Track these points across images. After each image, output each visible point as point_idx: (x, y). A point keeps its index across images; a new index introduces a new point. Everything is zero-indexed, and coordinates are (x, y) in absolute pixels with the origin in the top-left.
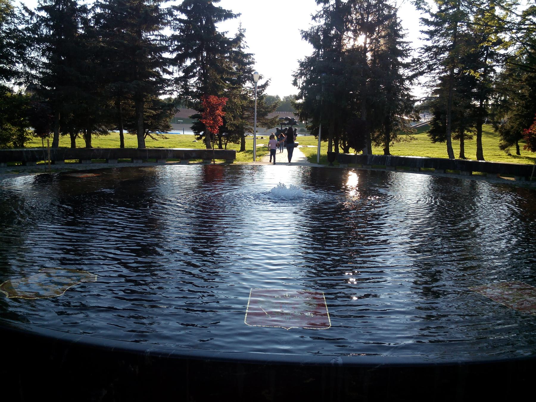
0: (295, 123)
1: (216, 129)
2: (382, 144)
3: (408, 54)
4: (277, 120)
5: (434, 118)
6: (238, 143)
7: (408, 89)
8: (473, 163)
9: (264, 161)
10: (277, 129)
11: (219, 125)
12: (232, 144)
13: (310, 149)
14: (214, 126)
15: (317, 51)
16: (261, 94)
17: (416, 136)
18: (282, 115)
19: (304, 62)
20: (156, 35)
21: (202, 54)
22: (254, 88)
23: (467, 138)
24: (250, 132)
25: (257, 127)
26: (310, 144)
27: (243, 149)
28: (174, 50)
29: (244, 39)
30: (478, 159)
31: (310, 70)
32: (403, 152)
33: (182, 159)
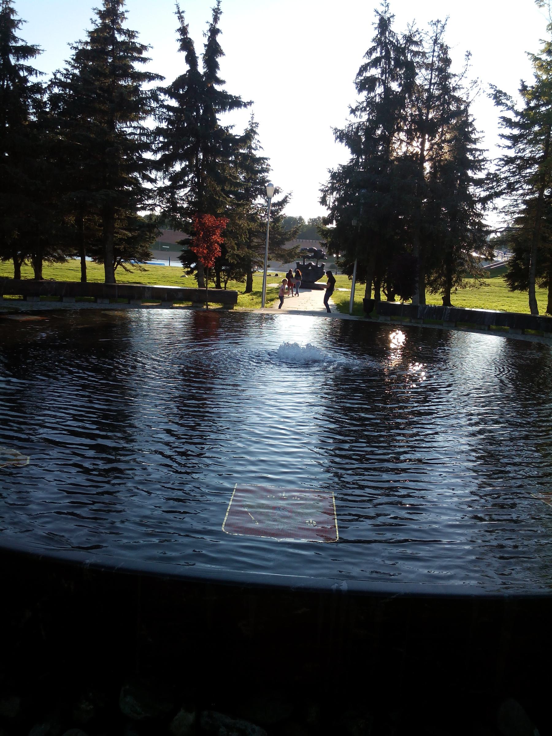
4: (298, 251)
6: (243, 282)
10: (298, 264)
11: (216, 255)
12: (234, 282)
13: (341, 294)
14: (209, 257)
16: (278, 214)
17: (488, 281)
19: (336, 173)
20: (134, 127)
24: (260, 266)
25: (269, 259)
26: (342, 287)
27: (249, 289)
32: (469, 302)
33: (163, 300)
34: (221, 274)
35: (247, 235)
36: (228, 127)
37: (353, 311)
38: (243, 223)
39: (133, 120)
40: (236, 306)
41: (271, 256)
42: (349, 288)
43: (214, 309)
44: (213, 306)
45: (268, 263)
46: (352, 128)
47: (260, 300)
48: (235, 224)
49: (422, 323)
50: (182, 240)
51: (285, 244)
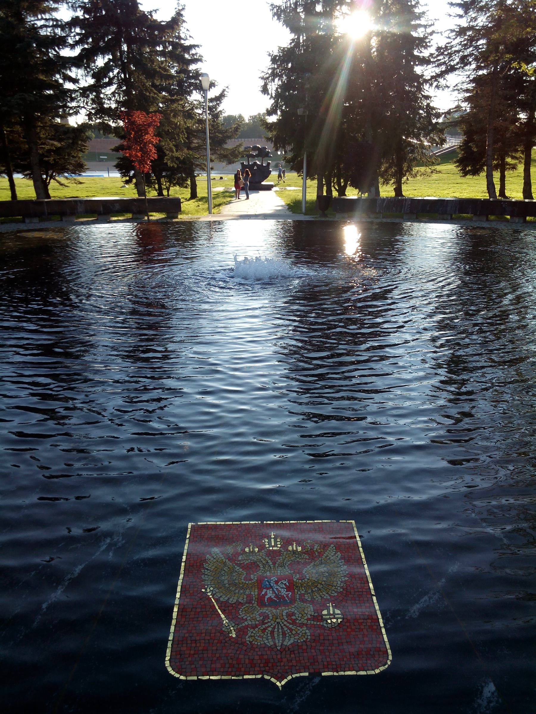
0: (267, 155)
1: (147, 165)
2: (392, 181)
3: (428, 44)
4: (242, 149)
5: (465, 140)
6: (186, 187)
7: (427, 97)
8: (518, 203)
9: (225, 213)
10: (242, 164)
11: (151, 158)
12: (177, 188)
13: (290, 193)
14: (144, 161)
15: (296, 37)
16: (216, 110)
17: (438, 168)
18: (249, 143)
19: (277, 56)
20: (46, 20)
21: (120, 48)
22: (205, 102)
23: (510, 169)
24: (203, 170)
25: (212, 161)
26: (289, 186)
27: (194, 195)
28: (77, 43)
29: (184, 25)
30: (525, 198)
31: (287, 69)
32: (420, 191)
33: (100, 214)
34: (162, 180)
35: (184, 134)
36: (151, 12)
37: (305, 210)
38: (179, 120)
39: (44, 12)
40: (181, 214)
41: (213, 157)
42: (300, 186)
43: (157, 220)
44: (156, 216)
45: (211, 165)
46: (290, 4)
47: (206, 206)
48: (170, 123)
49: (381, 217)
50: (116, 147)
51: (226, 143)
